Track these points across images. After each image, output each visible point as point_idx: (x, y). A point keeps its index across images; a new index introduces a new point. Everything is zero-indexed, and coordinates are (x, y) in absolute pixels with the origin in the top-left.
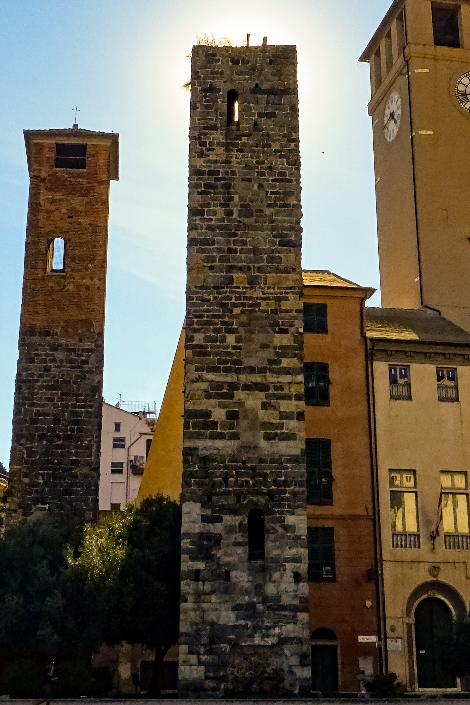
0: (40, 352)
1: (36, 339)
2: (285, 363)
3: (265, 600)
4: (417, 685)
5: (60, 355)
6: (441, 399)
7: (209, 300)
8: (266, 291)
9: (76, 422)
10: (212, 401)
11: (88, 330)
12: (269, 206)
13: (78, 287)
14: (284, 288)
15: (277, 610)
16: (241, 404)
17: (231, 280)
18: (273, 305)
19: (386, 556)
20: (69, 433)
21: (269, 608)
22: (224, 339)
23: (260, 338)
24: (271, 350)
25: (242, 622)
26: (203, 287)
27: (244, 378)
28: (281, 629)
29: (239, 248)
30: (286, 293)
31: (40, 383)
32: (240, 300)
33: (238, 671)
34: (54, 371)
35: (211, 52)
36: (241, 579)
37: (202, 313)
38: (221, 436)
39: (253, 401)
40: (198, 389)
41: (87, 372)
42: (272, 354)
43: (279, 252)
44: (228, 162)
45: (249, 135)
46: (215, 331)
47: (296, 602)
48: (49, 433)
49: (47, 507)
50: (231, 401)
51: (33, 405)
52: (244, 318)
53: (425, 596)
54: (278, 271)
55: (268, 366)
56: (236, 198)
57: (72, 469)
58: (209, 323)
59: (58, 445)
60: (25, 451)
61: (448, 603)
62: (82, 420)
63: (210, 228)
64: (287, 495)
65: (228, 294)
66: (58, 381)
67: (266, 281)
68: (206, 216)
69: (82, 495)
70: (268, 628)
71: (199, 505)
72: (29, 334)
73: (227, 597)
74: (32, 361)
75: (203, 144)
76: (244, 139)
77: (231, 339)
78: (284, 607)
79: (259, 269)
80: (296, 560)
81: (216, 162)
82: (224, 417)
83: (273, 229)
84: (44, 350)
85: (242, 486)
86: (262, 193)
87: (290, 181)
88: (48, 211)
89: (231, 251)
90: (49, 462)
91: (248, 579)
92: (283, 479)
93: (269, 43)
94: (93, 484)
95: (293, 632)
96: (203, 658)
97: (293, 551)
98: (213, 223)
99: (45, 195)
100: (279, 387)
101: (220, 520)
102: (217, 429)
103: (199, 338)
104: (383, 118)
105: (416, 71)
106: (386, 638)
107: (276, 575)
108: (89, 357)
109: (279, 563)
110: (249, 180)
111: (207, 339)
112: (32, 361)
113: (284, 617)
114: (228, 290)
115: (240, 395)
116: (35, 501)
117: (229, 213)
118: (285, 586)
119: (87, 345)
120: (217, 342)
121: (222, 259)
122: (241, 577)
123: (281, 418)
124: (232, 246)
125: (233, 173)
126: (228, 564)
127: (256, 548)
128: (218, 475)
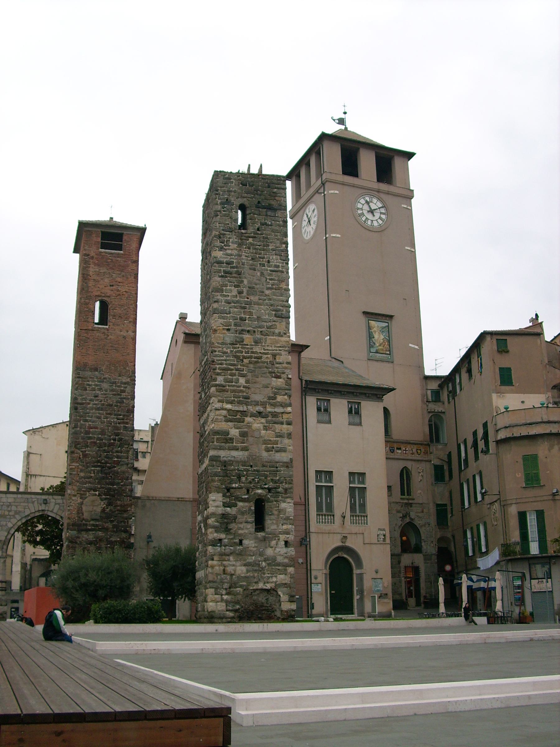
0: (90, 383)
2: (279, 398)
4: (329, 614)
5: (105, 386)
6: (350, 424)
8: (266, 348)
9: (117, 435)
10: (230, 423)
12: (268, 289)
14: (278, 347)
15: (274, 565)
16: (249, 426)
19: (312, 530)
20: (112, 441)
23: (263, 381)
26: (223, 343)
30: (281, 350)
31: (91, 405)
35: (227, 176)
38: (236, 449)
39: (257, 424)
40: (220, 415)
41: (125, 398)
42: (271, 392)
43: (274, 321)
46: (232, 375)
47: (286, 561)
49: (97, 493)
51: (86, 421)
53: (337, 555)
54: (273, 334)
56: (246, 282)
59: (105, 450)
61: (350, 560)
62: (121, 433)
65: (240, 349)
66: (103, 404)
68: (224, 293)
71: (221, 495)
72: (80, 370)
74: (86, 390)
76: (251, 240)
77: (242, 381)
78: (279, 564)
80: (287, 532)
82: (237, 434)
84: (92, 382)
85: (250, 483)
86: (264, 279)
87: (283, 272)
89: (243, 319)
90: (98, 461)
92: (278, 478)
93: (264, 172)
96: (225, 597)
97: (285, 527)
98: (229, 298)
100: (275, 415)
101: (235, 505)
104: (302, 222)
105: (330, 192)
106: (311, 583)
107: (273, 543)
108: (126, 388)
109: (275, 536)
110: (255, 270)
111: (226, 380)
112: (86, 390)
115: (248, 419)
118: (278, 550)
119: (125, 379)
120: (232, 382)
121: (236, 325)
123: (277, 437)
124: (243, 316)
127: (260, 524)
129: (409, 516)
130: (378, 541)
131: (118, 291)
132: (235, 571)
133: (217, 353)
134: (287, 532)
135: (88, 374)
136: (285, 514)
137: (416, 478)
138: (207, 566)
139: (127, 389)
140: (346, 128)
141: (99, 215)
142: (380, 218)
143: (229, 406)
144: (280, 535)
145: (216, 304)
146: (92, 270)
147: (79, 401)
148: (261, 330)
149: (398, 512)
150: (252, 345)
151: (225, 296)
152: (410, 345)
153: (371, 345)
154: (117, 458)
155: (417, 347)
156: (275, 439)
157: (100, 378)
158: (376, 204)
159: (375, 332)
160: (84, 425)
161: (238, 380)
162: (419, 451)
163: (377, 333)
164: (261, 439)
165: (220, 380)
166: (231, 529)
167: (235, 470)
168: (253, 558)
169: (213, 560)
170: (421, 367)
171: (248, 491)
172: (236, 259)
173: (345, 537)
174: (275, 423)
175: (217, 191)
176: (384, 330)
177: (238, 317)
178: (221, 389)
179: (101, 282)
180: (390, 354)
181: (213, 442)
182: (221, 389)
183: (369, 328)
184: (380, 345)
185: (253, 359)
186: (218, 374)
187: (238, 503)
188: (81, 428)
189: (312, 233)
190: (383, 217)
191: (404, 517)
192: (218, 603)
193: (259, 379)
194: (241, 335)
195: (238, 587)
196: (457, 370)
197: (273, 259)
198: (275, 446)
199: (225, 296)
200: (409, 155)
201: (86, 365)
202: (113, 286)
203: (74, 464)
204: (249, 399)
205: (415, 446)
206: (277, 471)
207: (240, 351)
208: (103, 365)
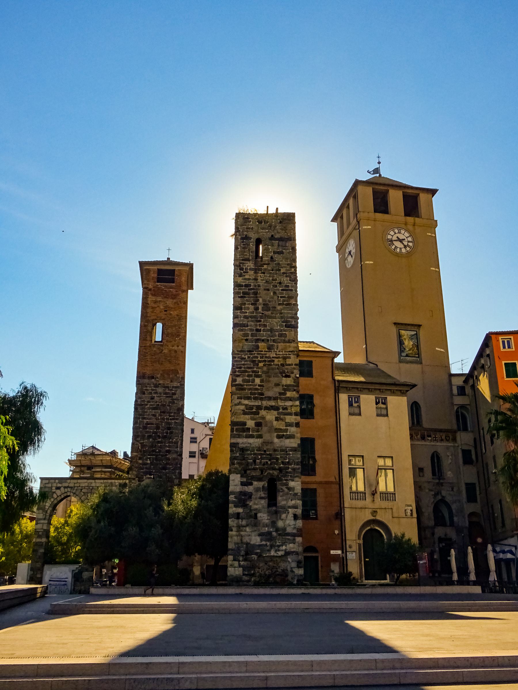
0: (148, 388)
1: (146, 381)
2: (289, 394)
3: (277, 530)
4: (364, 578)
5: (160, 390)
6: (378, 415)
7: (245, 358)
8: (278, 353)
9: (169, 428)
10: (247, 416)
11: (176, 375)
12: (279, 304)
13: (170, 351)
16: (263, 418)
17: (258, 347)
18: (281, 361)
21: (280, 535)
22: (253, 381)
24: (281, 387)
25: (264, 543)
26: (241, 351)
27: (265, 403)
29: (262, 329)
30: (289, 354)
34: (156, 399)
38: (252, 436)
39: (270, 416)
40: (239, 409)
41: (175, 399)
44: (256, 279)
45: (268, 264)
46: (248, 376)
47: (295, 531)
49: (152, 476)
52: (265, 369)
53: (369, 528)
54: (284, 342)
56: (261, 300)
57: (167, 455)
58: (245, 371)
60: (140, 445)
61: (382, 531)
63: (246, 317)
66: (158, 405)
70: (279, 546)
71: (239, 475)
73: (255, 528)
74: (144, 394)
75: (242, 269)
76: (265, 266)
77: (258, 381)
78: (288, 534)
79: (274, 341)
80: (295, 507)
81: (249, 279)
82: (253, 425)
83: (282, 318)
84: (150, 387)
85: (264, 465)
86: (276, 297)
87: (292, 290)
88: (153, 308)
89: (258, 330)
90: (153, 451)
92: (287, 460)
95: (293, 548)
96: (242, 563)
97: (293, 502)
98: (247, 314)
99: (151, 298)
100: (285, 408)
101: (251, 484)
103: (239, 380)
106: (346, 552)
107: (284, 516)
108: (176, 391)
109: (285, 509)
110: (268, 290)
111: (244, 381)
112: (144, 394)
115: (263, 413)
116: (146, 473)
117: (257, 309)
118: (289, 522)
119: (175, 384)
121: (252, 335)
122: (264, 517)
123: (286, 426)
124: (258, 328)
125: (259, 286)
126: (256, 509)
129: (441, 494)
137: (447, 462)
140: (380, 175)
141: (159, 255)
144: (290, 510)
146: (151, 298)
149: (430, 490)
152: (437, 349)
155: (442, 350)
156: (285, 428)
163: (407, 340)
170: (447, 366)
172: (253, 282)
173: (375, 512)
177: (255, 329)
180: (418, 357)
183: (400, 336)
184: (410, 350)
187: (253, 482)
189: (352, 262)
190: (411, 244)
191: (435, 495)
193: (271, 379)
196: (474, 368)
197: (283, 280)
200: (433, 192)
204: (263, 395)
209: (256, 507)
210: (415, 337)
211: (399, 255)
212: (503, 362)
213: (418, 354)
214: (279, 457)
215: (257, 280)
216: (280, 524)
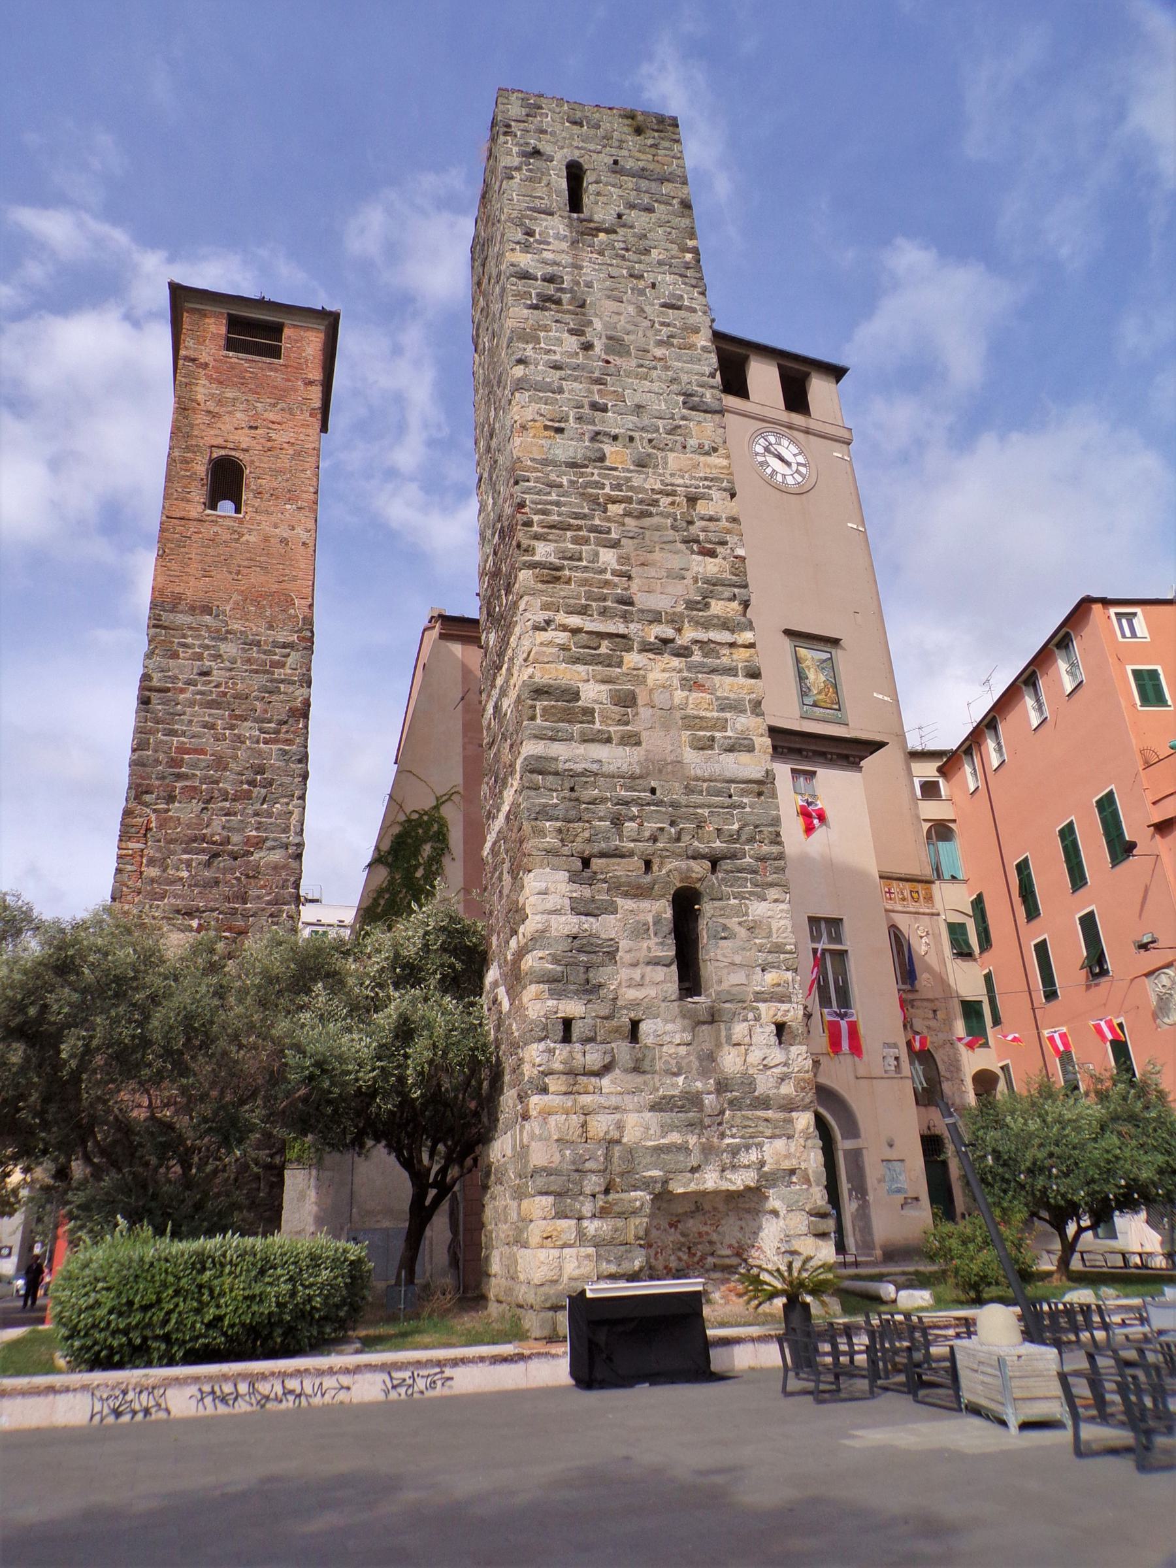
0: (189, 640)
2: (717, 608)
3: (722, 1087)
5: (229, 649)
7: (561, 486)
8: (669, 480)
10: (580, 668)
12: (660, 343)
13: (266, 539)
20: (245, 787)
25: (675, 1138)
28: (762, 1152)
30: (709, 488)
31: (188, 695)
32: (621, 491)
33: (657, 1253)
34: (217, 675)
36: (667, 1038)
37: (549, 507)
39: (661, 672)
41: (282, 681)
42: (692, 591)
46: (576, 540)
48: (204, 786)
49: (195, 923)
50: (619, 670)
51: (172, 733)
55: (686, 612)
56: (598, 324)
62: (272, 765)
64: (748, 859)
66: (225, 694)
67: (666, 464)
68: (542, 345)
69: (269, 903)
70: (735, 1151)
71: (563, 875)
73: (639, 1079)
77: (608, 557)
78: (764, 1103)
80: (780, 996)
82: (604, 698)
84: (199, 637)
91: (682, 1038)
94: (290, 884)
95: (788, 1156)
97: (771, 977)
98: (557, 357)
102: (594, 723)
107: (739, 1030)
109: (744, 1003)
112: (175, 656)
113: (765, 1124)
114: (596, 471)
117: (588, 347)
118: (755, 1053)
120: (580, 559)
121: (579, 419)
122: (665, 1031)
123: (722, 710)
126: (635, 1004)
128: (601, 814)
130: (886, 1072)
131: (270, 440)
132: (620, 1127)
133: (531, 484)
134: (780, 996)
135: (183, 619)
136: (769, 936)
138: (525, 1117)
139: (290, 660)
142: (797, 471)
143: (575, 621)
144: (761, 1005)
145: (522, 367)
147: (155, 683)
148: (650, 436)
150: (631, 471)
151: (548, 352)
153: (804, 693)
154: (257, 829)
156: (715, 714)
157: (218, 631)
158: (788, 450)
159: (808, 667)
160: (166, 742)
161: (597, 554)
162: (915, 895)
164: (678, 714)
165: (544, 551)
166: (600, 986)
167: (604, 800)
168: (680, 1080)
169: (544, 1090)
171: (648, 865)
174: (713, 671)
175: (509, 126)
176: (824, 665)
178: (552, 575)
179: (227, 418)
180: (839, 710)
181: (533, 718)
182: (552, 575)
183: (798, 660)
184: (820, 693)
185: (634, 506)
186: (537, 537)
187: (619, 901)
188: (156, 751)
190: (803, 470)
192: (566, 1251)
194: (597, 445)
195: (635, 1188)
198: (718, 735)
199: (548, 352)
201: (180, 598)
202: (256, 428)
203: (131, 845)
205: (908, 885)
206: (733, 806)
207: (597, 482)
208: (228, 601)
209: (632, 994)
210: (828, 665)
211: (782, 489)
212: (1129, 668)
213: (838, 703)
214: (705, 812)
215: (581, 268)
216: (730, 1061)
